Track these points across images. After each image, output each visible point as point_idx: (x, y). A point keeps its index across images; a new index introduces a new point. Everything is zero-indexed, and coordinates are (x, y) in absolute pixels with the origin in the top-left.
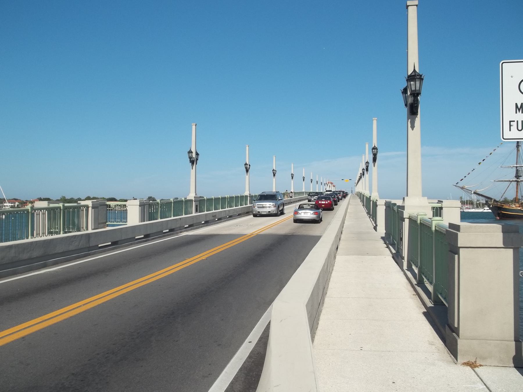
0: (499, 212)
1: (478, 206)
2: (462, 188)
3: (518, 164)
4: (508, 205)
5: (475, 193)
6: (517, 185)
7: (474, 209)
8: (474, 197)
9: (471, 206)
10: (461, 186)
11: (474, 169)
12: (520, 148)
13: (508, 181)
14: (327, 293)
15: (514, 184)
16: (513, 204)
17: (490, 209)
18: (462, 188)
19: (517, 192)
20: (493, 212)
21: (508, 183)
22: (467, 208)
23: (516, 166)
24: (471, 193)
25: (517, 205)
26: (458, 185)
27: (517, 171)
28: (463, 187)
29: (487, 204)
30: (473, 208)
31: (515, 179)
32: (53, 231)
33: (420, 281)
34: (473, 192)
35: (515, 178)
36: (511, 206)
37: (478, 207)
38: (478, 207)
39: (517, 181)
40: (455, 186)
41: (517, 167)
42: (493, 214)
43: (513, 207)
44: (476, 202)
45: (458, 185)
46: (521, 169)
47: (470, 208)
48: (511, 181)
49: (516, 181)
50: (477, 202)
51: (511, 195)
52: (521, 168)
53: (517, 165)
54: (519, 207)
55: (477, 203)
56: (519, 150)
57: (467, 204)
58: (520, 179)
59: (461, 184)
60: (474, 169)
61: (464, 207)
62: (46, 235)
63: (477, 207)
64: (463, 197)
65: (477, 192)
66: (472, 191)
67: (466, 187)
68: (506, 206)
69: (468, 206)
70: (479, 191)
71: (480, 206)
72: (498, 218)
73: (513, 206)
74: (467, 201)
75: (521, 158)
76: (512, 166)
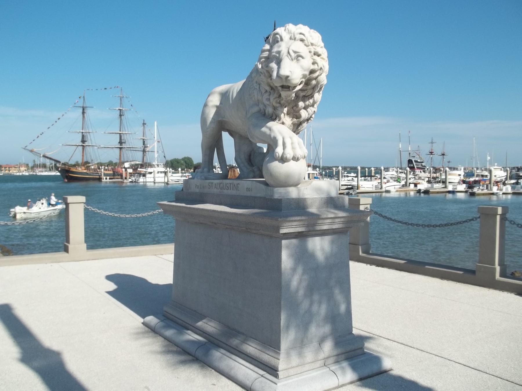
0: (67, 175)
1: (51, 170)
2: (31, 151)
3: (83, 129)
4: (75, 168)
5: (44, 156)
6: (83, 149)
7: (46, 172)
8: (48, 162)
9: (44, 170)
10: (30, 149)
11: (43, 133)
12: (85, 115)
13: (74, 145)
14: (46, 264)
15: (81, 148)
16: (80, 167)
17: (60, 172)
18: (31, 151)
19: (83, 156)
20: (62, 175)
21: (75, 147)
22: (40, 171)
23: (82, 131)
24: (40, 156)
25: (83, 168)
26: (27, 148)
27: (83, 136)
28: (32, 150)
29: (57, 168)
30: (46, 171)
31: (81, 144)
32: (484, 168)
33: (371, 210)
34: (42, 155)
35: (81, 142)
36: (78, 169)
37: (51, 171)
38: (51, 171)
39: (83, 146)
40: (24, 149)
41: (82, 132)
42: (61, 176)
43: (80, 169)
44: (49, 165)
45: (27, 148)
46: (86, 135)
47: (42, 172)
48: (78, 146)
49: (82, 145)
50: (50, 166)
51: (78, 158)
52: (87, 134)
53: (120, 131)
54: (85, 170)
55: (49, 167)
56: (84, 117)
57: (40, 167)
58: (85, 144)
59: (29, 148)
60: (43, 133)
61: (37, 170)
62: (218, 188)
63: (50, 170)
64: (36, 160)
65: (46, 156)
66: (41, 154)
67: (35, 150)
68: (73, 170)
69: (41, 169)
70: (48, 154)
71: (53, 169)
72: (66, 180)
73: (80, 169)
74: (40, 164)
75: (86, 123)
76: (78, 131)
